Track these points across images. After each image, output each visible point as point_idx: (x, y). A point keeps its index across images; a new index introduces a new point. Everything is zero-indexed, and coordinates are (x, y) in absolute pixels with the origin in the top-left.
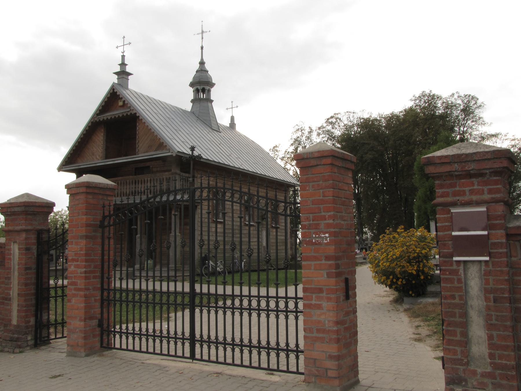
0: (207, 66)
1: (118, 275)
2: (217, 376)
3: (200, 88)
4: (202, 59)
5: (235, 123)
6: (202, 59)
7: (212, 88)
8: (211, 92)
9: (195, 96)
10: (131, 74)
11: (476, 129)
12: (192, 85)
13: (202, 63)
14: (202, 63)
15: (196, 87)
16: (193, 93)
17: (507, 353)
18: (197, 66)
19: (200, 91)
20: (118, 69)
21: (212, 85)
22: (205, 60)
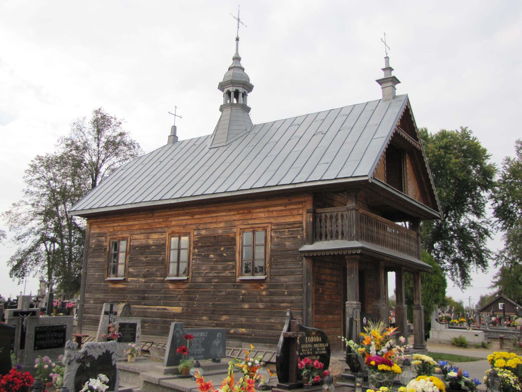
0: (243, 63)
1: (184, 255)
2: (162, 332)
3: (232, 89)
4: (237, 53)
5: (177, 135)
6: (237, 53)
7: (249, 92)
8: (248, 97)
9: (225, 101)
10: (399, 82)
11: (67, 176)
12: (221, 86)
13: (237, 59)
14: (237, 59)
15: (226, 90)
16: (223, 98)
17: (157, 367)
18: (230, 63)
19: (232, 94)
20: (382, 75)
21: (250, 88)
22: (241, 55)
